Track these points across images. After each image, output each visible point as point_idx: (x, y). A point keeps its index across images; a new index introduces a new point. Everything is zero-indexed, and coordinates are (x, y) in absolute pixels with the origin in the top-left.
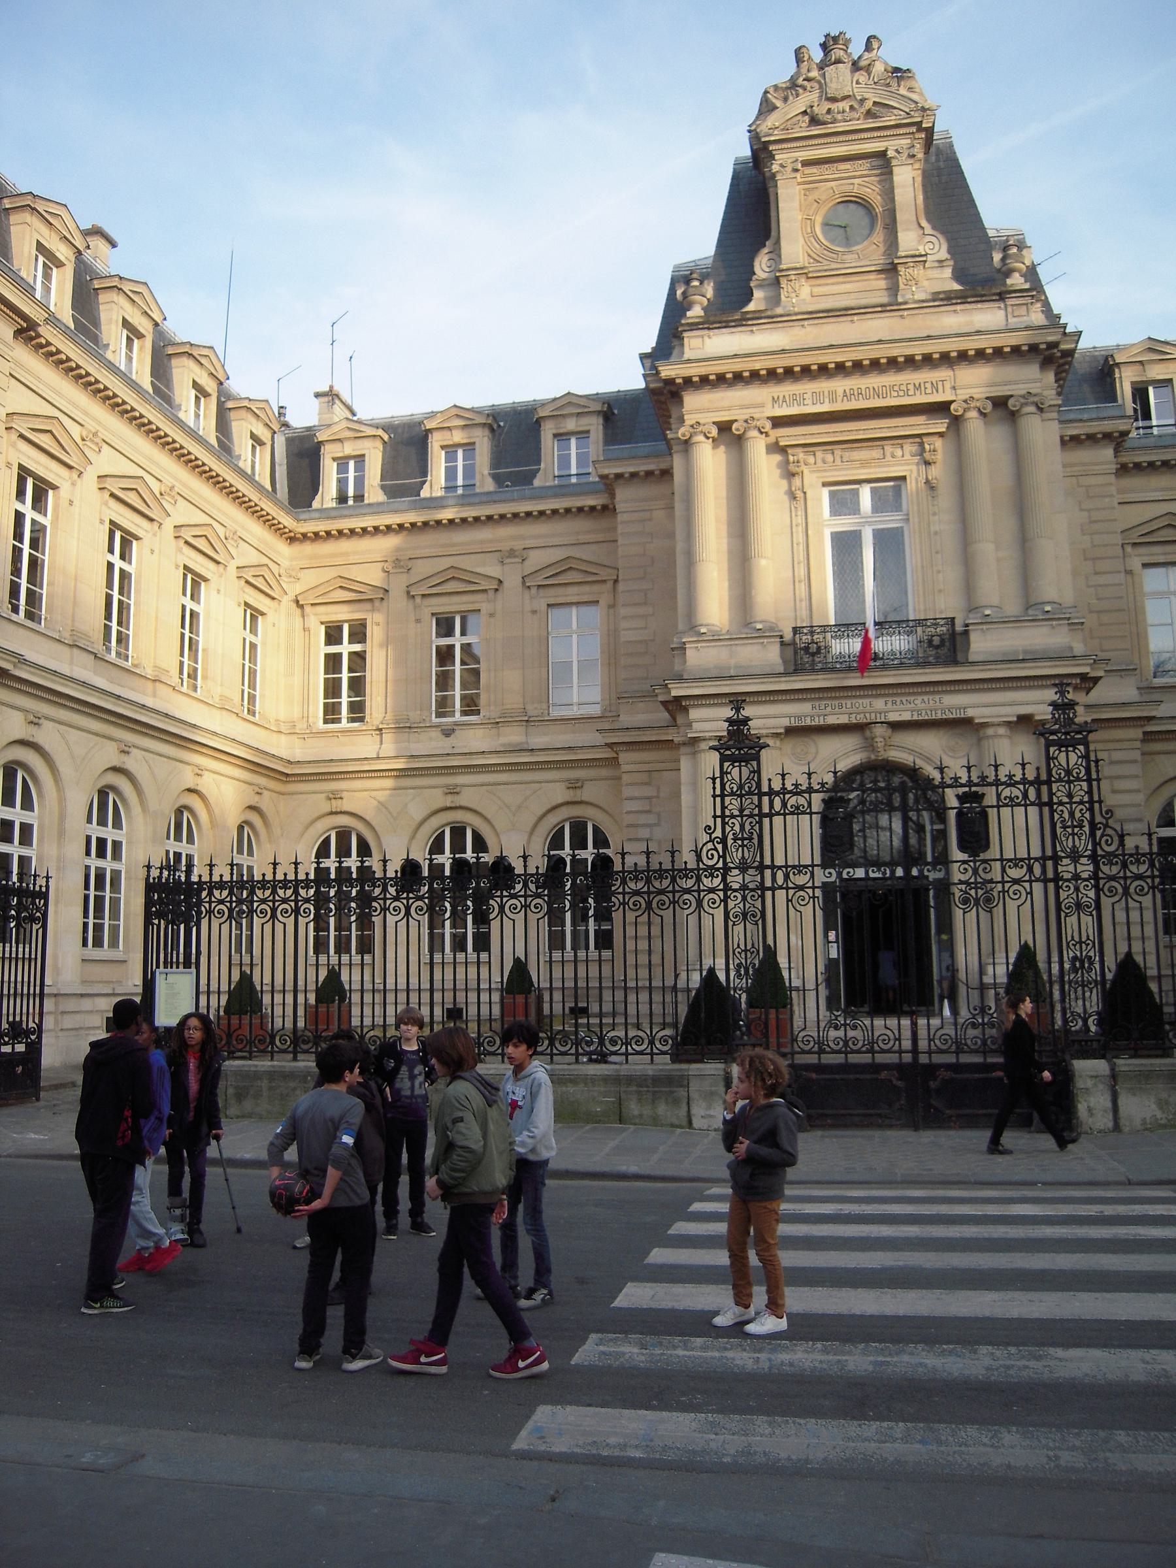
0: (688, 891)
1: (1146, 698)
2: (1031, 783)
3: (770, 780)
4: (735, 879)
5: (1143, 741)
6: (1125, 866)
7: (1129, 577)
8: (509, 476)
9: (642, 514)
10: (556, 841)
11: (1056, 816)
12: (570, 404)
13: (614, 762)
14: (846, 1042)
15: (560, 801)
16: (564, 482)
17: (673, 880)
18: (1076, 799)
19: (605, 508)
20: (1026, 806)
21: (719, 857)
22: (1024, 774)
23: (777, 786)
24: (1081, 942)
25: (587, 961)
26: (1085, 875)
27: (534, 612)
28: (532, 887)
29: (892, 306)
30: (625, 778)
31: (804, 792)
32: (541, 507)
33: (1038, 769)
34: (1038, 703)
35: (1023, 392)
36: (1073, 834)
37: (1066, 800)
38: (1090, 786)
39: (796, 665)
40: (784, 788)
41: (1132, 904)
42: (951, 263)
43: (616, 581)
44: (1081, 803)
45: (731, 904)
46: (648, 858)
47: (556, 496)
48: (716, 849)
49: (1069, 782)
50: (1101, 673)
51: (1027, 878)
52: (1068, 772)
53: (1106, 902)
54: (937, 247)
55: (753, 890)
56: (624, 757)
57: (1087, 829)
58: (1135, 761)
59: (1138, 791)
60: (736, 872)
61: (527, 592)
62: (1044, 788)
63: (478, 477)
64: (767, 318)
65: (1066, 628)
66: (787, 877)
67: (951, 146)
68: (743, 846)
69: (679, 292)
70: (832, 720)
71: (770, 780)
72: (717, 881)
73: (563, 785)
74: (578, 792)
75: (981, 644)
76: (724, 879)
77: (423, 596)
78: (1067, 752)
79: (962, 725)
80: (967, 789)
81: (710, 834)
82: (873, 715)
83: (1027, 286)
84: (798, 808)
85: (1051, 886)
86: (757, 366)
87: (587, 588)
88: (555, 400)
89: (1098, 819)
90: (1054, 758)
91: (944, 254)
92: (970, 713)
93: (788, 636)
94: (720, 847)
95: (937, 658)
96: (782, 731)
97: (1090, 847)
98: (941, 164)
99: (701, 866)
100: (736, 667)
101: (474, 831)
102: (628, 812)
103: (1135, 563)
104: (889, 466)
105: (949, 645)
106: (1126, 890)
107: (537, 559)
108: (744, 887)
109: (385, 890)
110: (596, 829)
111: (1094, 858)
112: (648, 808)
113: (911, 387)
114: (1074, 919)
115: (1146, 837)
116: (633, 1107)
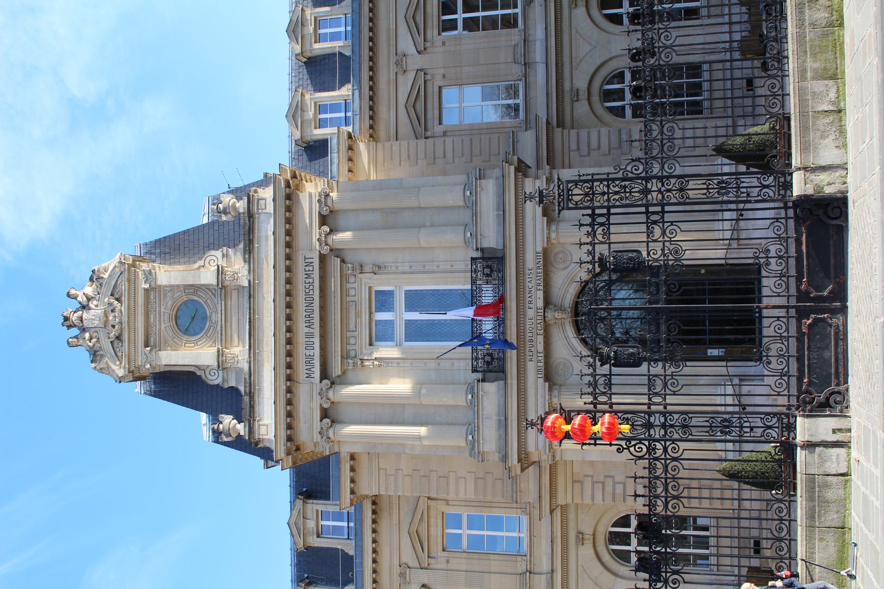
1: (533, 124)
2: (594, 220)
3: (585, 403)
4: (657, 433)
6: (658, 497)
7: (448, 134)
11: (618, 203)
13: (564, 508)
14: (780, 257)
15: (592, 551)
17: (657, 459)
18: (606, 190)
19: (374, 503)
21: (640, 443)
22: (587, 225)
23: (590, 399)
25: (718, 537)
27: (448, 561)
29: (251, 292)
30: (577, 500)
31: (593, 229)
35: (317, 204)
36: (630, 192)
37: (606, 197)
38: (597, 180)
40: (591, 394)
41: (685, 494)
42: (225, 248)
43: (429, 498)
44: (608, 186)
45: (676, 436)
48: (635, 445)
49: (593, 194)
50: (515, 158)
51: (661, 225)
52: (586, 195)
53: (679, 171)
54: (213, 258)
56: (561, 501)
57: (627, 183)
58: (578, 134)
59: (599, 131)
60: (649, 197)
61: (428, 50)
62: (597, 211)
64: (252, 378)
65: (482, 181)
66: (656, 394)
67: (146, 244)
68: (630, 192)
69: (226, 439)
70: (541, 348)
71: (585, 403)
72: (659, 446)
73: (581, 548)
74: (586, 537)
75: (491, 241)
76: (658, 441)
77: (425, 40)
78: (572, 195)
79: (547, 258)
80: (596, 264)
81: (624, 449)
84: (606, 384)
87: (432, 521)
88: (292, 534)
89: (620, 175)
90: (576, 204)
91: (218, 253)
92: (539, 249)
93: (479, 376)
94: (633, 443)
95: (499, 271)
96: (547, 384)
98: (158, 251)
99: (647, 456)
100: (499, 415)
102: (603, 500)
103: (439, 129)
105: (490, 263)
106: (674, 497)
107: (408, 557)
108: (663, 426)
111: (647, 179)
116: (832, 518)
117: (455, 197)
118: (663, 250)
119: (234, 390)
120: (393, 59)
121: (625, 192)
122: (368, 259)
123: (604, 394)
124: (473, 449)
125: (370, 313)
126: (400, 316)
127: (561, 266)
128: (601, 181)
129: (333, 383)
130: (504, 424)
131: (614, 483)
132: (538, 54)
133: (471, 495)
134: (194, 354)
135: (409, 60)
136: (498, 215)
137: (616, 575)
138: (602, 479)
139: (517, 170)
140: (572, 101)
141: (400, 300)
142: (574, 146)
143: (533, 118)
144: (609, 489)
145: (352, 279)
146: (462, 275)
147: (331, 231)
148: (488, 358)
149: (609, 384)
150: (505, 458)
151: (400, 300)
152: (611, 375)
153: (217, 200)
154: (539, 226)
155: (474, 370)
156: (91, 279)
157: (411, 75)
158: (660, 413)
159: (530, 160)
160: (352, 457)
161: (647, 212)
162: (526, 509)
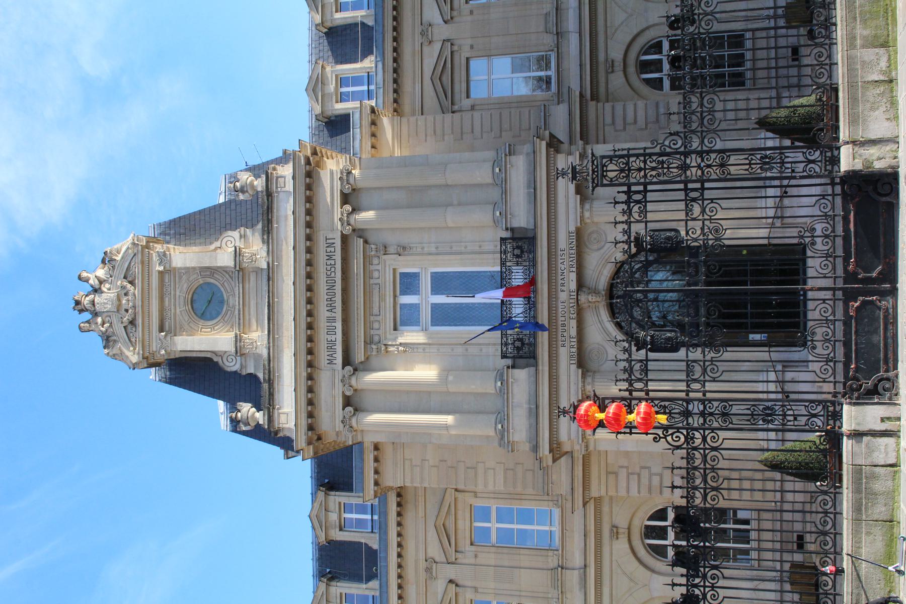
0: (705, 456)
2: (629, 197)
3: (620, 390)
4: (696, 421)
5: (598, 100)
7: (477, 107)
8: (369, 568)
9: (406, 467)
10: (660, 551)
11: (655, 180)
12: (318, 520)
13: (598, 501)
15: (627, 546)
16: (377, 525)
17: (695, 449)
18: (642, 165)
19: (399, 495)
20: (646, 202)
21: (678, 432)
23: (625, 385)
24: (750, 164)
26: (699, 160)
27: (476, 556)
28: (697, 581)
29: (270, 274)
30: (612, 493)
31: (629, 206)
32: (390, 28)
33: (619, 192)
34: (565, 188)
36: (668, 168)
37: (642, 173)
38: (633, 155)
39: (530, 358)
40: (626, 380)
42: (242, 229)
43: (456, 490)
44: (645, 162)
45: (715, 425)
46: (677, 487)
47: (386, 533)
48: (672, 434)
49: (629, 170)
50: (547, 133)
51: (700, 202)
52: (622, 171)
53: (719, 145)
55: (705, 407)
56: (594, 493)
57: (665, 158)
58: (613, 107)
59: (635, 105)
60: (688, 173)
61: (455, 19)
62: (633, 188)
63: (367, 593)
64: (271, 364)
66: (696, 381)
67: (160, 224)
68: (668, 168)
69: (244, 428)
70: (574, 332)
73: (615, 542)
74: (620, 531)
75: (521, 220)
76: (696, 429)
78: (607, 171)
79: (580, 238)
80: (632, 244)
81: (660, 438)
82: (571, 301)
83: (264, 176)
85: (707, 185)
86: (304, 374)
87: (460, 513)
88: (313, 528)
89: (657, 150)
91: (236, 234)
92: (572, 228)
93: (509, 362)
94: (670, 431)
95: (530, 252)
96: (580, 371)
97: (678, 156)
98: (172, 232)
99: (685, 446)
100: (529, 404)
101: (645, 54)
102: (639, 492)
104: (385, 283)
105: (520, 244)
107: (435, 551)
108: (702, 414)
109: (696, 586)
110: (650, 519)
111: (686, 154)
112: (636, 477)
113: (329, 262)
114: (732, 168)
115: (675, 588)
116: (879, 511)
117: (483, 174)
118: (702, 229)
119: (253, 377)
120: (418, 29)
121: (663, 167)
122: (392, 239)
123: (640, 380)
124: (502, 438)
125: (395, 296)
126: (426, 299)
127: (595, 247)
128: (637, 156)
129: (355, 370)
130: (534, 412)
131: (651, 475)
132: (571, 23)
133: (500, 487)
134: (211, 340)
135: (436, 31)
136: (529, 193)
137: (653, 571)
138: (637, 470)
139: (549, 145)
140: (607, 73)
141: (426, 283)
142: (608, 120)
143: (565, 90)
144: (645, 481)
145: (375, 261)
146: (491, 256)
147: (354, 210)
148: (518, 344)
149: (645, 370)
150: (535, 448)
151: (426, 283)
152: (647, 360)
153: (234, 178)
154: (571, 205)
155: (504, 356)
156: (103, 261)
157: (437, 46)
158: (699, 400)
159: (562, 135)
160: (376, 447)
161: (686, 189)
162: (557, 501)
